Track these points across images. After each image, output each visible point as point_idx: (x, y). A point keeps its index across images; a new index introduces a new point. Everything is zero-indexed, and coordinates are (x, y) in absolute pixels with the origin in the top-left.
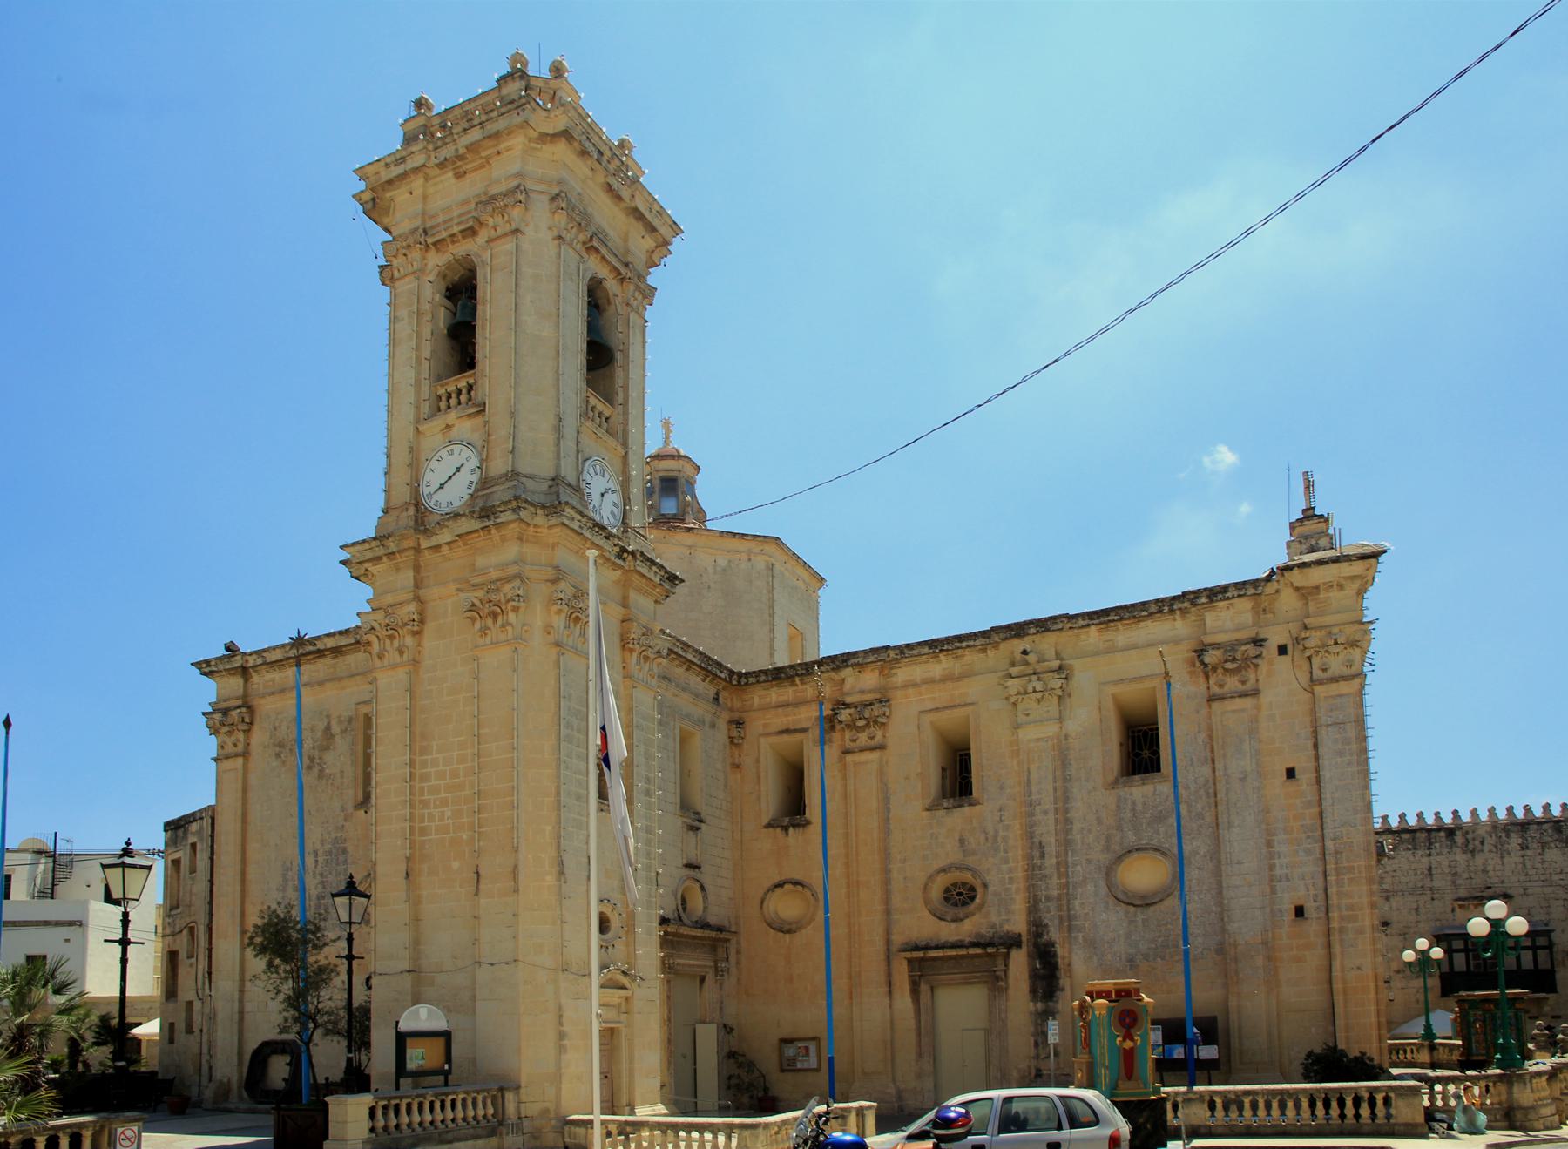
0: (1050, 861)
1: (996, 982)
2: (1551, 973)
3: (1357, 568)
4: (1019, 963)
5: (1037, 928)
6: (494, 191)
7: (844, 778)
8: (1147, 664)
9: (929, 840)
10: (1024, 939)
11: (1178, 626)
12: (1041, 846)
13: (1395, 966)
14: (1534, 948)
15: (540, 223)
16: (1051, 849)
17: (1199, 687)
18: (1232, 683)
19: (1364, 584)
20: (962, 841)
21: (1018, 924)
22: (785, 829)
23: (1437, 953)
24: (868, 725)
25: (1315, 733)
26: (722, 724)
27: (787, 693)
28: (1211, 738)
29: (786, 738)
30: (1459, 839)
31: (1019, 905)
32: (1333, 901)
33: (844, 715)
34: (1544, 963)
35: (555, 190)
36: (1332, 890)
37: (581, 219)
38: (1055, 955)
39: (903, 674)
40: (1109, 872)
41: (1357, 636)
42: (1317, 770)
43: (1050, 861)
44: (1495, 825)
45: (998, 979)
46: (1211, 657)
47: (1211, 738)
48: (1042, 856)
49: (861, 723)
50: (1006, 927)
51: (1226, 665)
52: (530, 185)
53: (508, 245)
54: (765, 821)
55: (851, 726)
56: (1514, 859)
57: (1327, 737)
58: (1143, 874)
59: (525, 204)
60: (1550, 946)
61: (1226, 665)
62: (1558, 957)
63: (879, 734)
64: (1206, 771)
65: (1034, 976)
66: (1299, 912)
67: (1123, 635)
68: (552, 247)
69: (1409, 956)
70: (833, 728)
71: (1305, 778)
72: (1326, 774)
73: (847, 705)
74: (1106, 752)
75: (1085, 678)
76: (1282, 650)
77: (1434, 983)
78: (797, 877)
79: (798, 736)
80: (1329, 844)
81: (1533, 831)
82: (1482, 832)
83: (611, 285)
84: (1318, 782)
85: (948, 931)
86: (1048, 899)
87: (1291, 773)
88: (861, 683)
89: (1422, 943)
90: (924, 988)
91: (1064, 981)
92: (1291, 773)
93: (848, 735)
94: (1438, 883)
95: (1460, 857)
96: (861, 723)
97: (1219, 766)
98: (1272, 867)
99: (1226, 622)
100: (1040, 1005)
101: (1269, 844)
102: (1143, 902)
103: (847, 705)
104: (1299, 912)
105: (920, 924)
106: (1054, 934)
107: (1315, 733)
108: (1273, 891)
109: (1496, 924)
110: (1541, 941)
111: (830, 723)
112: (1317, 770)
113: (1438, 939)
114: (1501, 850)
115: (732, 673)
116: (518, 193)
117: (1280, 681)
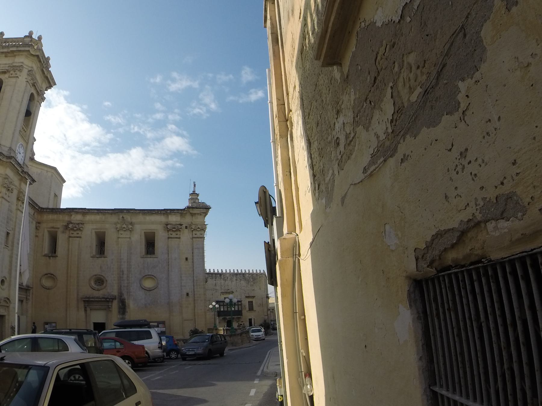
0: (125, 276)
1: (108, 309)
2: (241, 311)
3: (205, 211)
4: (115, 305)
5: (121, 294)
6: (15, 64)
7: (69, 244)
8: (155, 225)
9: (92, 266)
10: (117, 297)
11: (162, 219)
12: (123, 271)
13: (207, 309)
14: (238, 305)
15: (23, 77)
16: (125, 272)
17: (166, 234)
18: (174, 235)
19: (206, 214)
20: (101, 267)
21: (115, 293)
22: (49, 257)
23: (217, 306)
24: (77, 230)
25: (193, 250)
26: (34, 223)
27: (55, 217)
28: (168, 247)
29: (53, 230)
30: (222, 277)
31: (116, 287)
32: (196, 293)
33: (70, 226)
34: (240, 309)
35: (30, 69)
36: (195, 290)
37: (34, 78)
38: (125, 302)
39: (88, 218)
40: (140, 281)
41: (203, 228)
42: (193, 259)
43: (125, 276)
44: (230, 274)
45: (109, 308)
46: (169, 227)
47: (168, 247)
48: (123, 274)
49: (75, 229)
50: (112, 293)
51: (173, 230)
52: (24, 66)
53: (14, 80)
54: (43, 254)
55: (72, 229)
56: (234, 283)
57: (196, 251)
58: (148, 284)
59: (20, 71)
60: (241, 305)
61: (173, 230)
62: (243, 307)
63: (80, 232)
64: (167, 256)
65: (120, 308)
66: (188, 294)
67: (148, 218)
68: (25, 83)
69: (211, 306)
70: (67, 229)
71: (190, 260)
72: (195, 261)
73: (72, 223)
74: (141, 247)
75: (138, 228)
76: (186, 227)
77: (216, 313)
78: (52, 273)
79: (56, 230)
80: (195, 278)
81: (238, 276)
82: (228, 275)
83: (35, 95)
84: (193, 262)
85: (96, 294)
86: (124, 286)
87: (187, 259)
88: (78, 218)
89: (214, 303)
90: (88, 309)
91: (128, 310)
92: (187, 259)
93: (71, 232)
94: (218, 288)
95: (223, 281)
96: (75, 229)
97: (170, 255)
98: (181, 283)
99: (174, 219)
100: (121, 316)
101: (181, 277)
102: (150, 290)
103: (72, 223)
104: (188, 294)
105: (87, 291)
106: (125, 296)
107: (193, 250)
108: (181, 289)
109: (231, 300)
110: (240, 303)
111: (66, 227)
112: (193, 259)
113: (217, 302)
114: (231, 280)
115: (39, 207)
116: (20, 68)
117: (186, 235)
